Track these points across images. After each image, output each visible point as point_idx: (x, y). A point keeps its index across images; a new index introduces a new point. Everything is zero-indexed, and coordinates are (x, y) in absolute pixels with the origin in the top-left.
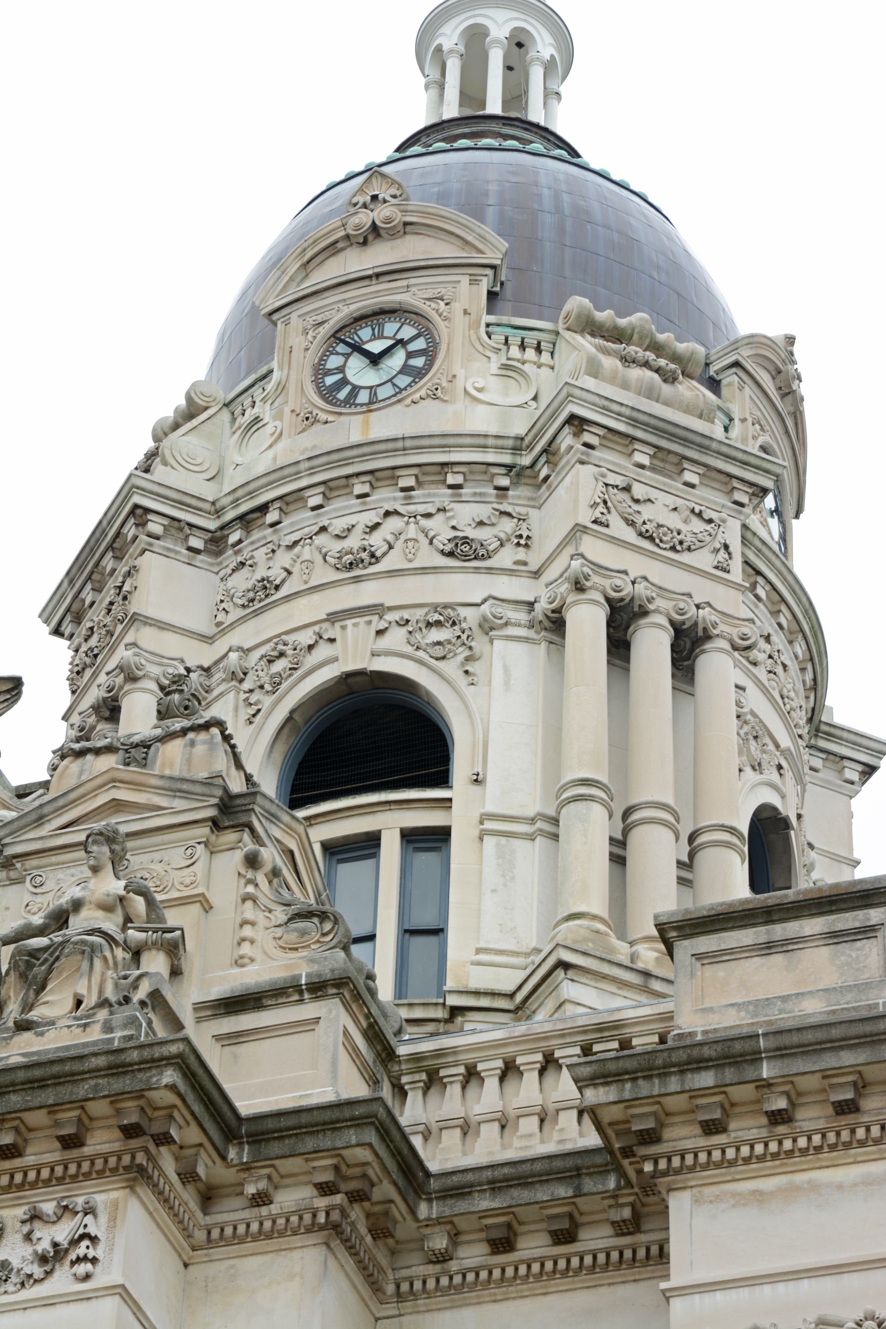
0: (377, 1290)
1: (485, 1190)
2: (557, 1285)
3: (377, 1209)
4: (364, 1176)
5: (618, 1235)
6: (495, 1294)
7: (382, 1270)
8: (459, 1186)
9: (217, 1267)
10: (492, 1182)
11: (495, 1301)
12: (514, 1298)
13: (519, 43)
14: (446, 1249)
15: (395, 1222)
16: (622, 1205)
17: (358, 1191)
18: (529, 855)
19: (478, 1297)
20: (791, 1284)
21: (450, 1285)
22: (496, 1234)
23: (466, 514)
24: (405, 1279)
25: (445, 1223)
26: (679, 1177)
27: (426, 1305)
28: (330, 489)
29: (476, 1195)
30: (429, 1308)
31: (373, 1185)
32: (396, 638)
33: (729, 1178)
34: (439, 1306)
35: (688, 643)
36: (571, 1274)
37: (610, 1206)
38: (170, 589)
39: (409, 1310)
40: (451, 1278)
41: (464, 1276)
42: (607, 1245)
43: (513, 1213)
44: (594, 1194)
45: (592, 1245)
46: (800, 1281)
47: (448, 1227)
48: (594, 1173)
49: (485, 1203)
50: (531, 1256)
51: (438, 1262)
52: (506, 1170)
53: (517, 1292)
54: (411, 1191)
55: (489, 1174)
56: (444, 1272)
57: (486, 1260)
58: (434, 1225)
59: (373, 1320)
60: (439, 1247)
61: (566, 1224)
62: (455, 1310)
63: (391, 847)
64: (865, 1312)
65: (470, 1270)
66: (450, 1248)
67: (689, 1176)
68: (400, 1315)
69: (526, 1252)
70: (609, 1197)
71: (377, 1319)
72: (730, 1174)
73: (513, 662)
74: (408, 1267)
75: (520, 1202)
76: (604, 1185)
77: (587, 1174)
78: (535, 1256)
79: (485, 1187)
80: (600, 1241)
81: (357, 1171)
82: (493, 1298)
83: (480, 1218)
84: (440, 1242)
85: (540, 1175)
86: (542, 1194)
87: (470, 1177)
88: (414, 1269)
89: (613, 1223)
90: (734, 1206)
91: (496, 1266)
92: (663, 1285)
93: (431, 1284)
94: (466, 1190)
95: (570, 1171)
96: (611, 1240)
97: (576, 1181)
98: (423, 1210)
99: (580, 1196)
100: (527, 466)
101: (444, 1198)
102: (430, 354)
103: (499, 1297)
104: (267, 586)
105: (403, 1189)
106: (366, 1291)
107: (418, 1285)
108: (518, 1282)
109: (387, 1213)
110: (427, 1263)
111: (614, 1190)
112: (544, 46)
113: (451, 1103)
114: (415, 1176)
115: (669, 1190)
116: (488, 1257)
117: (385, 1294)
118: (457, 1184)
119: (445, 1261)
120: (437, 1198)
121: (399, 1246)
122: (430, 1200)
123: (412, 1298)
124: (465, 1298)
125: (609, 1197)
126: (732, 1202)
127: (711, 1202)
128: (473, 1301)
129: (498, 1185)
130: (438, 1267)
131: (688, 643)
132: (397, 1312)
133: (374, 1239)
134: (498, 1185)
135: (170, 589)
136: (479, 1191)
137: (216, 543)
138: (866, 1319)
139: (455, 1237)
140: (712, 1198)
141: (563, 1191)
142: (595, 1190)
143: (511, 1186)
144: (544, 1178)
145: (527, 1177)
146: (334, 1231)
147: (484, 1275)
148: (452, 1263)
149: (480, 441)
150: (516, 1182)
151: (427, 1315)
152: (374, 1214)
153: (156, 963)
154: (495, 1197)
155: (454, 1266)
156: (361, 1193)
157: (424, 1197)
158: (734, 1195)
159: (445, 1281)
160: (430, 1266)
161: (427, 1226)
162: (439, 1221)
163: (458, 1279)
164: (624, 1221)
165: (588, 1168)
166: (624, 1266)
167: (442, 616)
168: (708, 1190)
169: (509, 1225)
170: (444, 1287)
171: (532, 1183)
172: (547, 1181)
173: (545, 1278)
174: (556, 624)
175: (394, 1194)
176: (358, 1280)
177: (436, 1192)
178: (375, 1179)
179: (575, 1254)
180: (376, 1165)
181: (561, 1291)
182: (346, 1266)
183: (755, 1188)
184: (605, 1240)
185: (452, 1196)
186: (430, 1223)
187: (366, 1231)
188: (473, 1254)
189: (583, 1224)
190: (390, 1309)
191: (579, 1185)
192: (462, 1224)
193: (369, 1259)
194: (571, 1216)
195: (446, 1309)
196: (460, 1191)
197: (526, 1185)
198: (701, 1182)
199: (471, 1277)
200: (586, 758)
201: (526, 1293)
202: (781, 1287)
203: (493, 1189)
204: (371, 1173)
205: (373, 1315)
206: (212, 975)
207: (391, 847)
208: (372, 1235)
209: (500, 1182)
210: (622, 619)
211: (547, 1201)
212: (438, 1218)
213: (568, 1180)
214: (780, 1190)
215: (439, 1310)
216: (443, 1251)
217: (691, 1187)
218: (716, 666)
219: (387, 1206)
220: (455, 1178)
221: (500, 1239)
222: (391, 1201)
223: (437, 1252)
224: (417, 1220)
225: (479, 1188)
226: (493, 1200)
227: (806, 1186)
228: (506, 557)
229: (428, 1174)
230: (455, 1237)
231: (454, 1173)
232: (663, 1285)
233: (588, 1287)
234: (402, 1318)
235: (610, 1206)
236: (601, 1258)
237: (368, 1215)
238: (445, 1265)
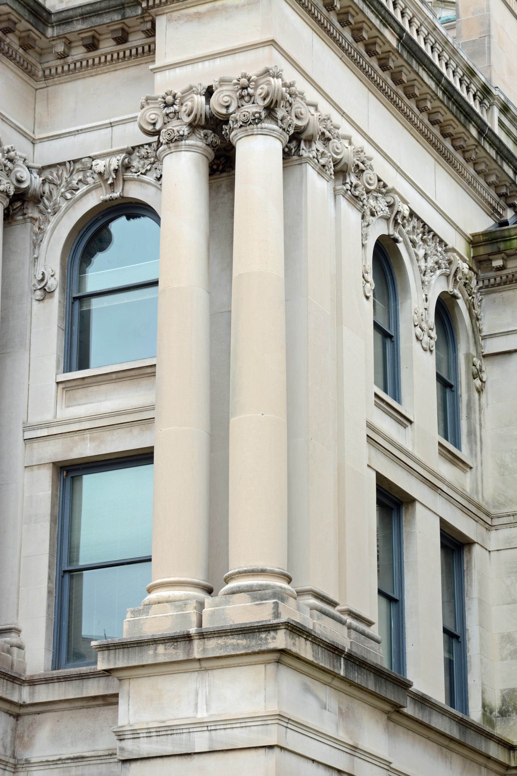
0: (33, 75)
1: (79, 19)
2: (120, 66)
3: (24, 34)
4: (9, 19)
5: (147, 37)
6: (91, 72)
7: (33, 65)
8: (66, 18)
10: (81, 15)
11: (92, 76)
12: (101, 74)
14: (64, 52)
15: (35, 40)
16: (147, 22)
17: (6, 28)
19: (83, 74)
20: (211, 61)
21: (69, 70)
22: (87, 42)
24: (47, 68)
25: (62, 38)
26: (160, 9)
27: (59, 81)
29: (75, 22)
30: (61, 82)
31: (15, 23)
33: (184, 7)
34: (65, 81)
36: (126, 59)
37: (141, 23)
39: (51, 84)
40: (69, 66)
41: (75, 64)
42: (142, 43)
43: (95, 30)
44: (131, 17)
45: (135, 44)
46: (216, 59)
47: (64, 40)
48: (131, 6)
49: (79, 26)
50: (106, 52)
51: (62, 58)
52: (88, 8)
53: (102, 70)
54: (40, 24)
55: (79, 11)
56: (66, 63)
57: (85, 56)
58: (56, 40)
59: (34, 90)
60: (60, 51)
61: (120, 34)
62: (73, 82)
64: (242, 74)
65: (78, 61)
66: (66, 50)
67: (164, 7)
68: (47, 87)
69: (104, 50)
70: (140, 18)
71: (36, 90)
72: (184, 5)
74: (48, 62)
75: (96, 24)
76: (136, 12)
77: (128, 7)
78: (108, 51)
79: (79, 18)
80: (138, 41)
81: (5, 17)
82: (90, 75)
83: (79, 34)
84: (60, 48)
85: (105, 9)
86: (106, 19)
87: (71, 13)
88: (50, 62)
89: (143, 31)
90: (186, 22)
91: (90, 58)
92: (151, 67)
93: (60, 70)
94: (70, 20)
95: (119, 6)
96: (144, 40)
97: (122, 11)
98: (50, 32)
99: (125, 19)
101: (59, 25)
103: (93, 74)
105: (34, 24)
106: (26, 77)
107: (53, 71)
108: (102, 65)
109: (28, 36)
110: (57, 59)
111: (141, 14)
114: (42, 16)
115: (156, 15)
116: (86, 54)
117: (37, 77)
118: (65, 17)
119: (65, 57)
120: (56, 25)
121: (43, 51)
122: (53, 27)
123: (51, 77)
124: (77, 76)
125: (140, 18)
126: (186, 19)
127: (176, 20)
128: (81, 77)
129: (85, 16)
130: (62, 61)
132: (45, 85)
133: (25, 50)
134: (85, 16)
136: (76, 20)
138: (242, 77)
139: (69, 44)
140: (176, 18)
141: (116, 17)
142: (131, 15)
143: (91, 16)
144: (107, 11)
145: (98, 11)
147: (84, 63)
148: (68, 58)
150: (93, 14)
151: (60, 85)
152: (23, 37)
154: (84, 23)
155: (70, 59)
156: (8, 29)
157: (50, 25)
158: (187, 15)
159: (66, 68)
160: (58, 61)
161: (53, 40)
162: (59, 37)
163: (72, 66)
164: (148, 30)
165: (128, 3)
166: (145, 55)
168: (175, 14)
169: (93, 37)
170: (66, 71)
171: (101, 14)
172: (109, 12)
173: (114, 62)
175: (30, 27)
176: (20, 72)
177: (55, 22)
178: (16, 20)
179: (128, 49)
180: (14, 13)
181: (123, 68)
182: (9, 66)
183: (196, 11)
184: (141, 40)
185: (63, 24)
186: (53, 39)
187: (18, 47)
188: (78, 53)
189: (131, 33)
190: (42, 84)
191: (124, 13)
192: (71, 37)
193: (24, 60)
194: (123, 29)
195: (69, 82)
196: (67, 21)
197: (98, 15)
198: (171, 10)
199: (78, 65)
201: (106, 71)
202: (207, 63)
203: (83, 18)
204: (13, 17)
205: (34, 88)
208: (23, 49)
209: (86, 14)
211: (109, 23)
212: (57, 36)
213: (119, 11)
214: (209, 11)
215: (66, 82)
216: (62, 53)
217: (167, 13)
219: (28, 32)
220: (64, 14)
221: (89, 44)
222: (30, 30)
223: (59, 53)
224: (47, 38)
225: (76, 19)
226: (83, 25)
227: (221, 8)
229: (49, 13)
230: (69, 44)
231: (63, 11)
232: (151, 67)
233: (136, 65)
234: (49, 88)
235: (141, 23)
236: (140, 50)
237: (20, 38)
238: (65, 60)
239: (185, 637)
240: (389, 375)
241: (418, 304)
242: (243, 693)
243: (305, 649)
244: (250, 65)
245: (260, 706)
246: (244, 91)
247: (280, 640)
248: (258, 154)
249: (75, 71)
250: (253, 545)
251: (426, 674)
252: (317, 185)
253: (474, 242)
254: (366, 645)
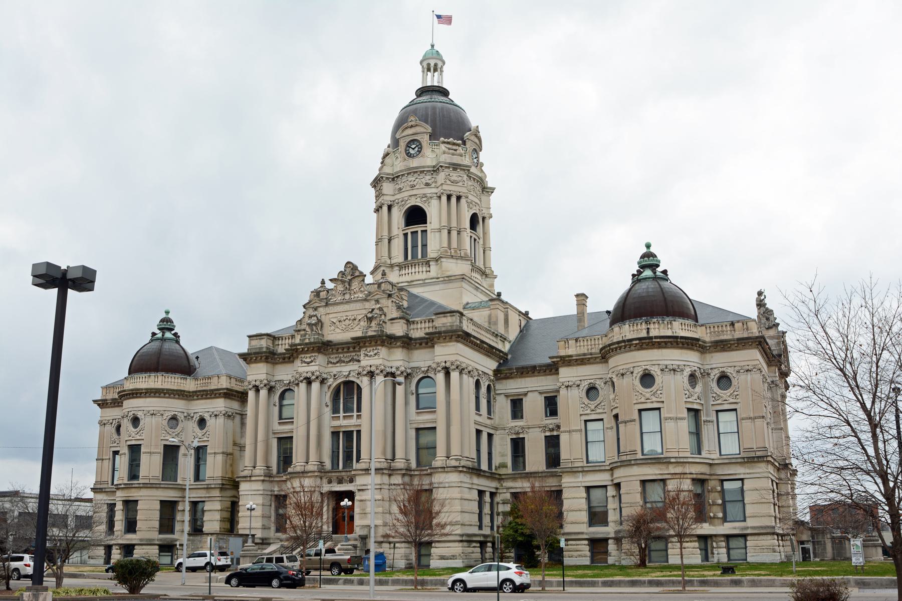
8: (416, 339)
9: (392, 350)
13: (436, 65)
18: (437, 234)
23: (428, 177)
28: (408, 174)
32: (419, 199)
35: (459, 198)
38: (387, 188)
63: (420, 233)
73: (434, 202)
100: (436, 170)
102: (421, 148)
104: (400, 189)
112: (440, 64)
113: (415, 326)
131: (459, 198)
135: (387, 188)
137: (393, 179)
146: (403, 347)
149: (428, 167)
153: (383, 317)
167: (425, 196)
174: (440, 197)
200: (444, 223)
206: (389, 317)
207: (420, 233)
210: (449, 197)
218: (463, 201)
228: (433, 185)
239: (706, 550)
240: (478, 408)
241: (483, 390)
242: (454, 477)
243: (465, 469)
244: (453, 358)
245: (261, 488)
246: (452, 364)
247: (461, 469)
248: (454, 375)
249: (417, 349)
250: (455, 451)
251: (484, 466)
252: (465, 377)
253: (494, 371)
254: (469, 251)
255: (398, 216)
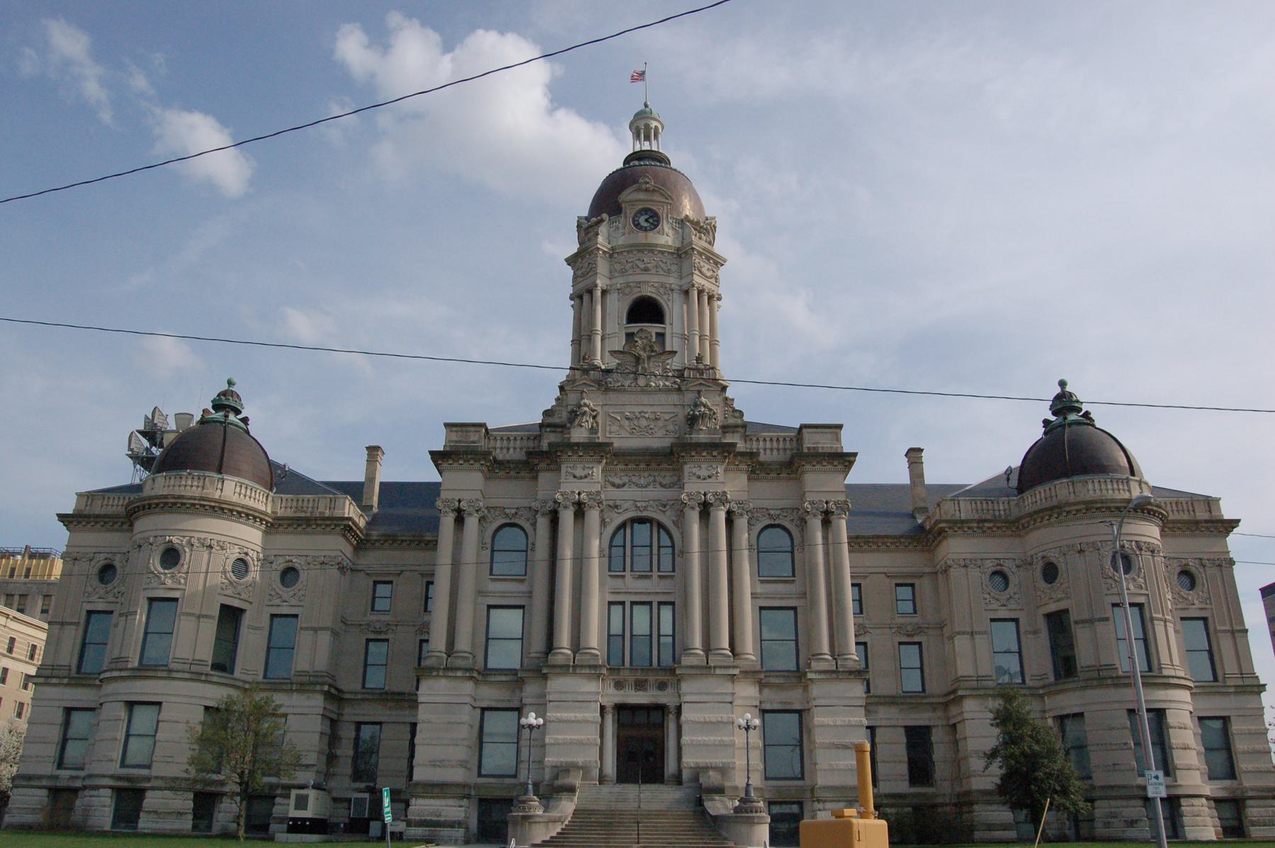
167: (663, 285)
255: (618, 307)
